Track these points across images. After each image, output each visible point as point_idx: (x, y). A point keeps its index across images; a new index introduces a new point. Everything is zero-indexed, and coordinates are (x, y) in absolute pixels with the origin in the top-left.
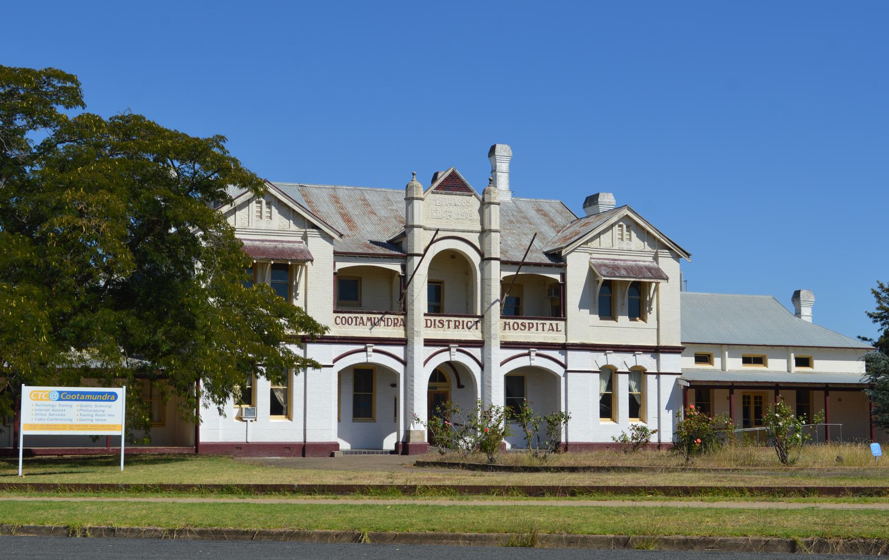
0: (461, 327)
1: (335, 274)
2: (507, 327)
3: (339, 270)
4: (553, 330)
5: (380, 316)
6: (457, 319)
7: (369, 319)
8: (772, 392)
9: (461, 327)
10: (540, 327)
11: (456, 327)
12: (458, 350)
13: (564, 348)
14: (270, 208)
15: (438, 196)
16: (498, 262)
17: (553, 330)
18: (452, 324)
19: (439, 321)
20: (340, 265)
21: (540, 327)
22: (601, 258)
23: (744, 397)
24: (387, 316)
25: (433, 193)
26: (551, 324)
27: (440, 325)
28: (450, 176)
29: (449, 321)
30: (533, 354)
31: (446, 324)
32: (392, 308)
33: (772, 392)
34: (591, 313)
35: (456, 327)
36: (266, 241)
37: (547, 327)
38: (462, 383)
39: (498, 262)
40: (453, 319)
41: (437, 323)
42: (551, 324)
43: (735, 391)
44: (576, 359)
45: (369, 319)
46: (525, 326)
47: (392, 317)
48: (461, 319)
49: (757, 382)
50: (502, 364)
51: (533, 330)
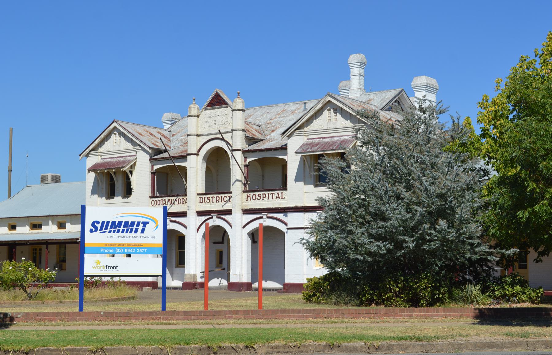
0: (220, 201)
1: (153, 173)
2: (249, 198)
3: (156, 170)
4: (279, 198)
5: (175, 198)
6: (218, 195)
7: (169, 200)
8: (44, 246)
9: (220, 201)
10: (270, 196)
11: (217, 201)
12: (218, 217)
13: (285, 210)
14: (336, 113)
15: (207, 111)
16: (240, 153)
17: (279, 198)
18: (215, 200)
19: (258, 196)
20: (156, 167)
21: (270, 196)
22: (315, 138)
23: (34, 249)
24: (179, 197)
25: (205, 110)
26: (278, 193)
27: (208, 201)
28: (215, 95)
29: (213, 197)
30: (265, 217)
31: (211, 199)
32: (167, 194)
33: (44, 246)
34: (305, 184)
35: (217, 201)
36: (126, 156)
37: (275, 196)
38: (256, 240)
39: (240, 153)
40: (215, 196)
41: (206, 199)
42: (278, 193)
43: (49, 246)
44: (294, 219)
45: (169, 200)
46: (260, 197)
47: (181, 198)
48: (220, 196)
49: (56, 240)
50: (244, 227)
51: (266, 199)
